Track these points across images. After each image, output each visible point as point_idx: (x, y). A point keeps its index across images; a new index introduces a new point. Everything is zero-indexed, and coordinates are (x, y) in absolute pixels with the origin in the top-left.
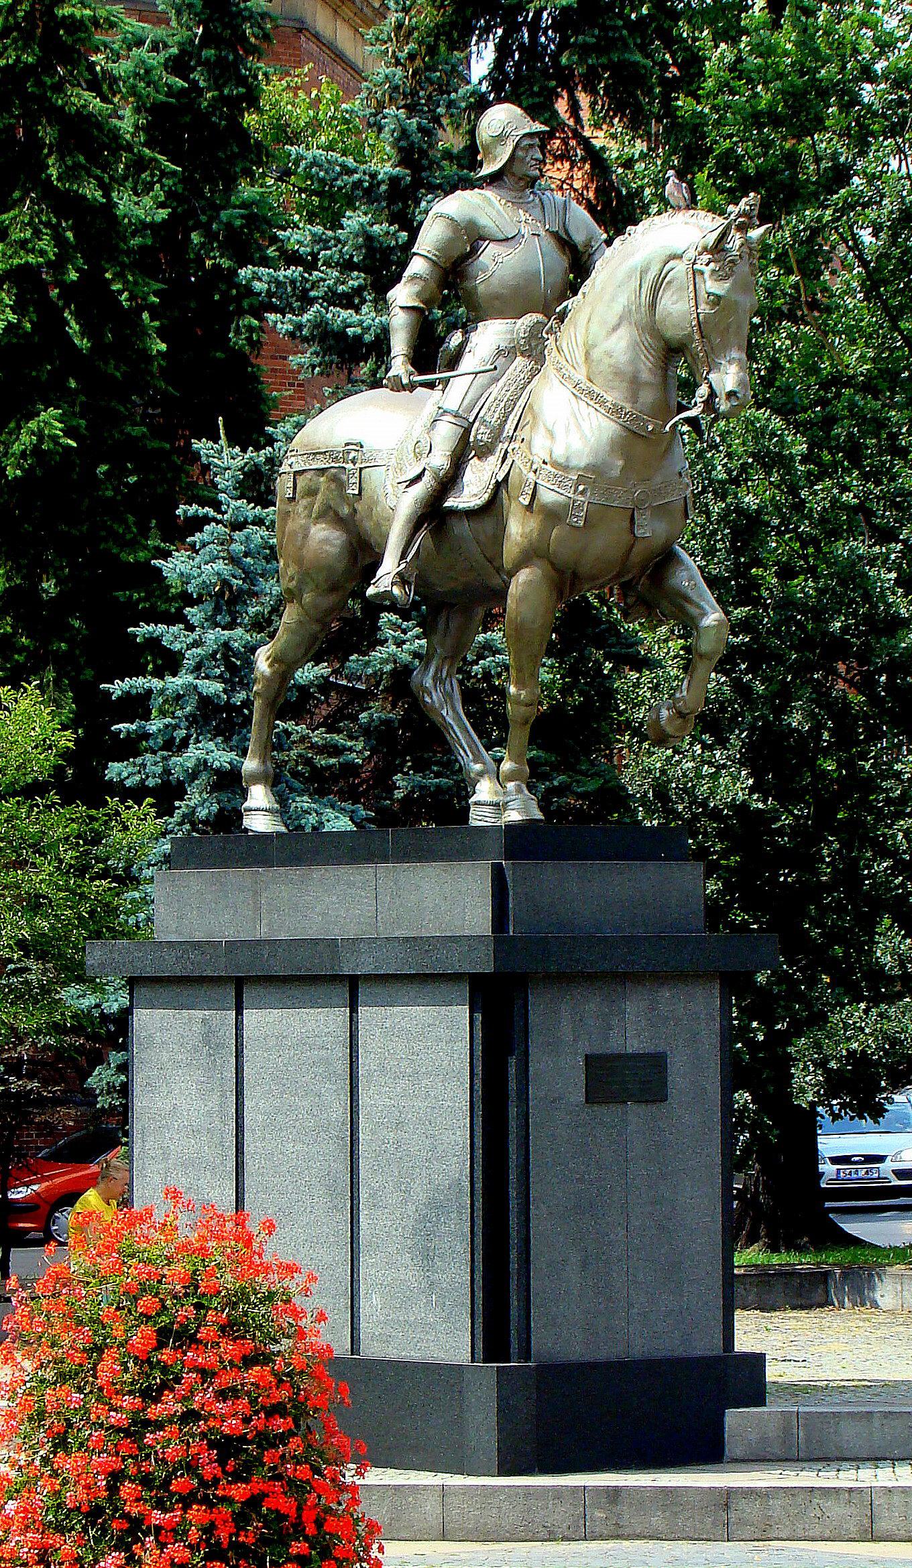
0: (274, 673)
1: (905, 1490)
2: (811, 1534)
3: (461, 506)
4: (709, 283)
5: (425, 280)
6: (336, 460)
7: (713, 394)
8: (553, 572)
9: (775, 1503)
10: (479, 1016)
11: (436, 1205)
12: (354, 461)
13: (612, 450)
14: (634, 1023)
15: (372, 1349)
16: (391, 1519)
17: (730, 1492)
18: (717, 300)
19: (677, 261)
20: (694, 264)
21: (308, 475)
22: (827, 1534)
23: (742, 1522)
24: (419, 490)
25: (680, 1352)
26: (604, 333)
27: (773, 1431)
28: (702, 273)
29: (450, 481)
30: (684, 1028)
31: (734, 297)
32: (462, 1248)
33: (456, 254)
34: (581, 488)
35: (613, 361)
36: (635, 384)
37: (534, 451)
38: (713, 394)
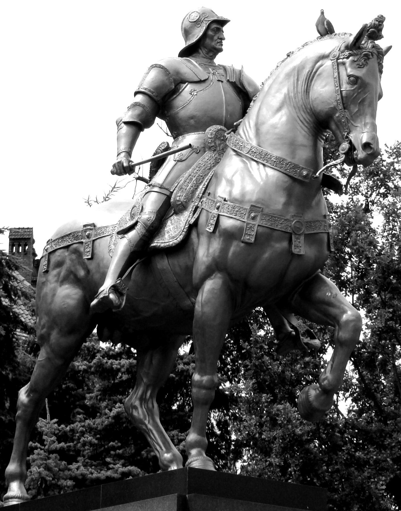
0: (30, 401)
5: (143, 106)
12: (88, 237)
21: (58, 253)
28: (344, 64)
29: (155, 228)
33: (165, 91)
34: (253, 215)
38: (352, 148)
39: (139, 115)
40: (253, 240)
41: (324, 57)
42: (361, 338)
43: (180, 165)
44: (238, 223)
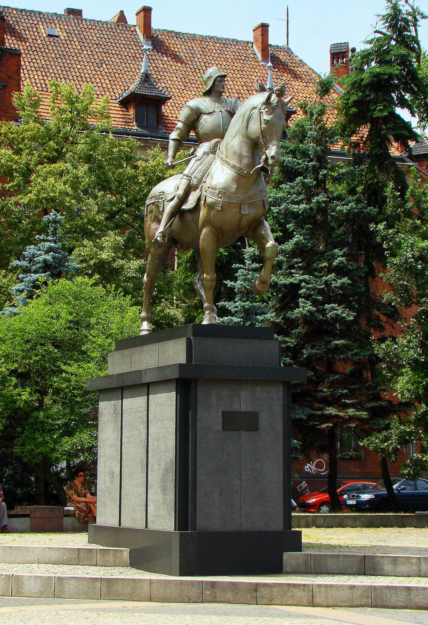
0: (148, 281)
1: (424, 589)
2: (289, 603)
3: (186, 208)
4: (265, 116)
7: (267, 158)
8: (214, 230)
9: (275, 590)
10: (178, 396)
11: (166, 470)
13: (232, 182)
14: (244, 401)
15: (151, 526)
16: (132, 592)
17: (257, 585)
18: (267, 122)
22: (295, 603)
23: (262, 597)
24: (173, 203)
25: (264, 529)
27: (301, 561)
29: (184, 199)
30: (269, 405)
31: (275, 121)
32: (173, 485)
33: (192, 119)
35: (233, 149)
36: (241, 157)
38: (267, 158)
39: (178, 135)
40: (220, 209)
41: (255, 108)
43: (198, 163)
44: (213, 200)
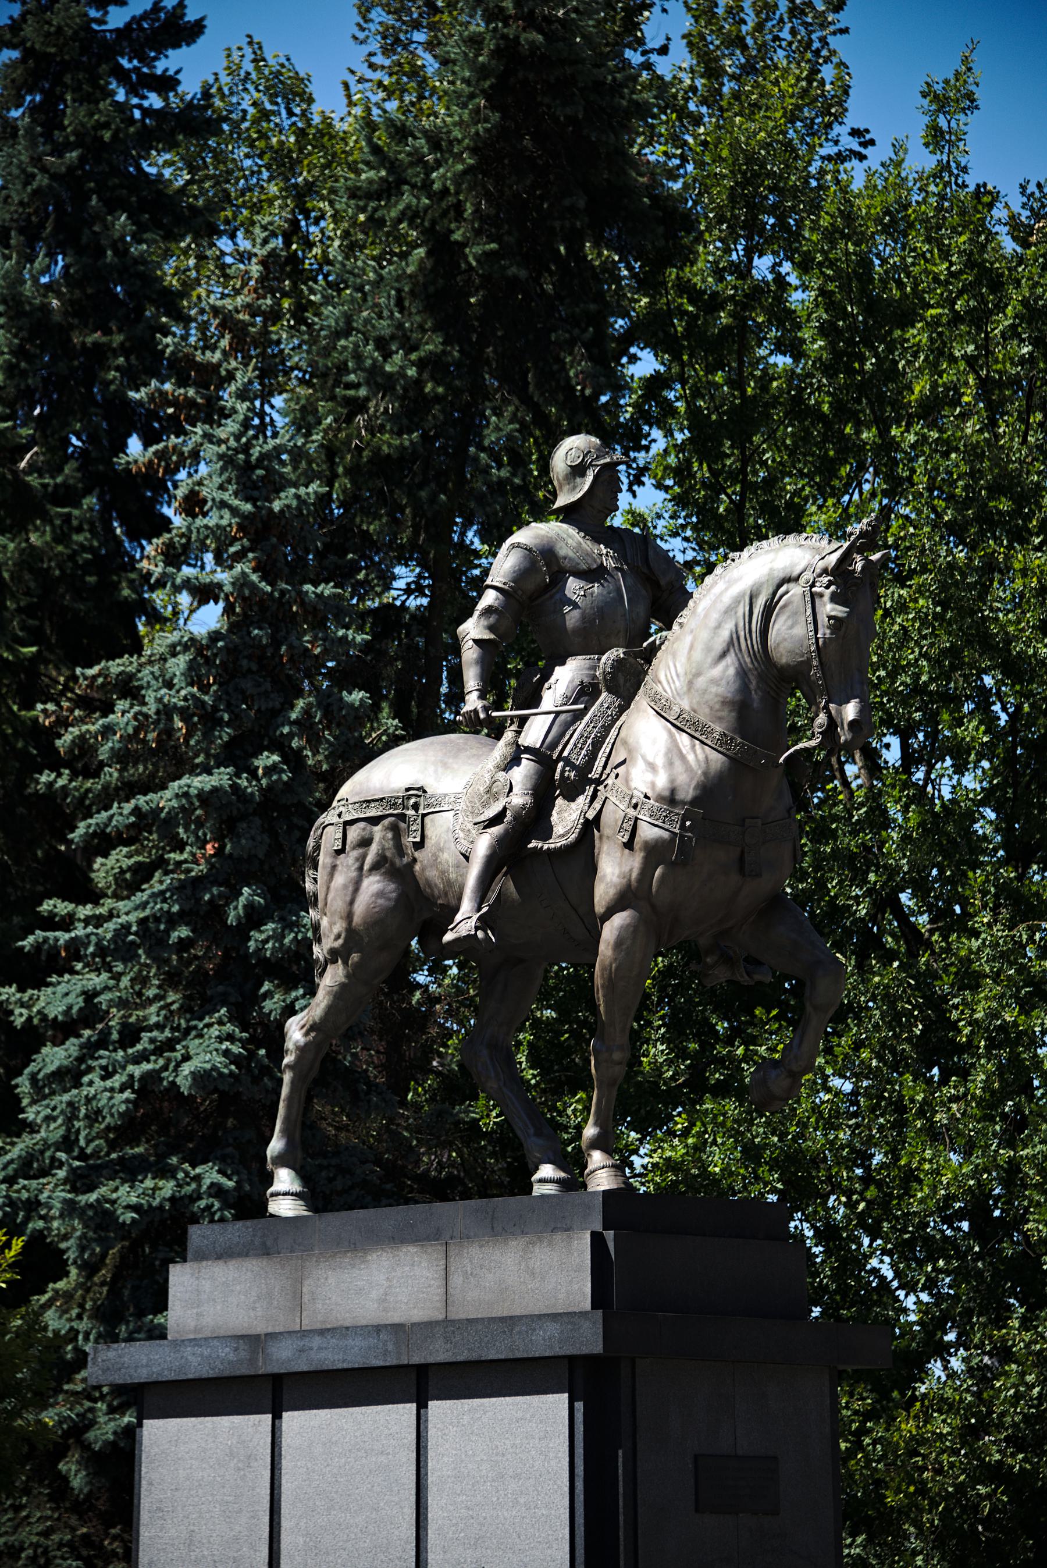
6: (394, 805)
12: (416, 807)
19: (791, 585)
20: (813, 585)
26: (709, 660)
37: (633, 785)
42: (972, 706)
44: (666, 835)
